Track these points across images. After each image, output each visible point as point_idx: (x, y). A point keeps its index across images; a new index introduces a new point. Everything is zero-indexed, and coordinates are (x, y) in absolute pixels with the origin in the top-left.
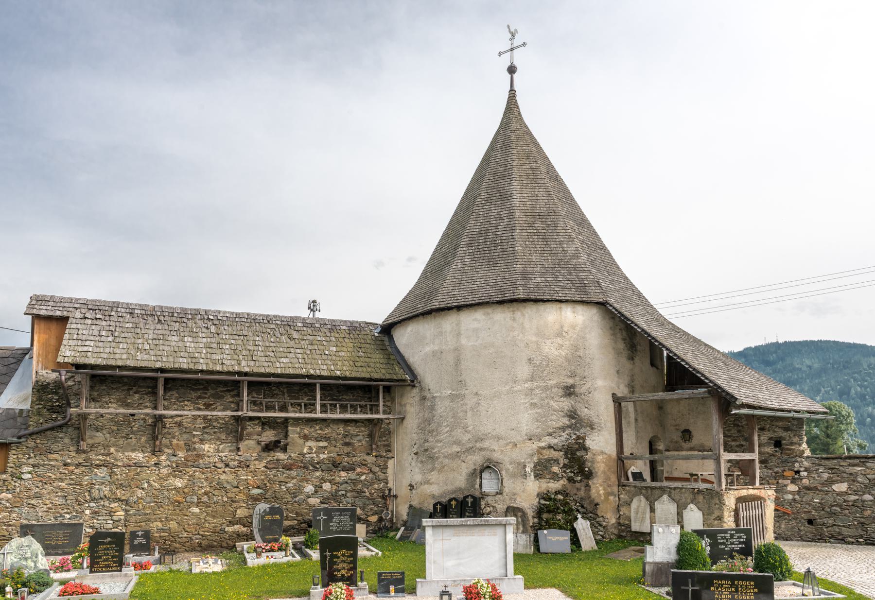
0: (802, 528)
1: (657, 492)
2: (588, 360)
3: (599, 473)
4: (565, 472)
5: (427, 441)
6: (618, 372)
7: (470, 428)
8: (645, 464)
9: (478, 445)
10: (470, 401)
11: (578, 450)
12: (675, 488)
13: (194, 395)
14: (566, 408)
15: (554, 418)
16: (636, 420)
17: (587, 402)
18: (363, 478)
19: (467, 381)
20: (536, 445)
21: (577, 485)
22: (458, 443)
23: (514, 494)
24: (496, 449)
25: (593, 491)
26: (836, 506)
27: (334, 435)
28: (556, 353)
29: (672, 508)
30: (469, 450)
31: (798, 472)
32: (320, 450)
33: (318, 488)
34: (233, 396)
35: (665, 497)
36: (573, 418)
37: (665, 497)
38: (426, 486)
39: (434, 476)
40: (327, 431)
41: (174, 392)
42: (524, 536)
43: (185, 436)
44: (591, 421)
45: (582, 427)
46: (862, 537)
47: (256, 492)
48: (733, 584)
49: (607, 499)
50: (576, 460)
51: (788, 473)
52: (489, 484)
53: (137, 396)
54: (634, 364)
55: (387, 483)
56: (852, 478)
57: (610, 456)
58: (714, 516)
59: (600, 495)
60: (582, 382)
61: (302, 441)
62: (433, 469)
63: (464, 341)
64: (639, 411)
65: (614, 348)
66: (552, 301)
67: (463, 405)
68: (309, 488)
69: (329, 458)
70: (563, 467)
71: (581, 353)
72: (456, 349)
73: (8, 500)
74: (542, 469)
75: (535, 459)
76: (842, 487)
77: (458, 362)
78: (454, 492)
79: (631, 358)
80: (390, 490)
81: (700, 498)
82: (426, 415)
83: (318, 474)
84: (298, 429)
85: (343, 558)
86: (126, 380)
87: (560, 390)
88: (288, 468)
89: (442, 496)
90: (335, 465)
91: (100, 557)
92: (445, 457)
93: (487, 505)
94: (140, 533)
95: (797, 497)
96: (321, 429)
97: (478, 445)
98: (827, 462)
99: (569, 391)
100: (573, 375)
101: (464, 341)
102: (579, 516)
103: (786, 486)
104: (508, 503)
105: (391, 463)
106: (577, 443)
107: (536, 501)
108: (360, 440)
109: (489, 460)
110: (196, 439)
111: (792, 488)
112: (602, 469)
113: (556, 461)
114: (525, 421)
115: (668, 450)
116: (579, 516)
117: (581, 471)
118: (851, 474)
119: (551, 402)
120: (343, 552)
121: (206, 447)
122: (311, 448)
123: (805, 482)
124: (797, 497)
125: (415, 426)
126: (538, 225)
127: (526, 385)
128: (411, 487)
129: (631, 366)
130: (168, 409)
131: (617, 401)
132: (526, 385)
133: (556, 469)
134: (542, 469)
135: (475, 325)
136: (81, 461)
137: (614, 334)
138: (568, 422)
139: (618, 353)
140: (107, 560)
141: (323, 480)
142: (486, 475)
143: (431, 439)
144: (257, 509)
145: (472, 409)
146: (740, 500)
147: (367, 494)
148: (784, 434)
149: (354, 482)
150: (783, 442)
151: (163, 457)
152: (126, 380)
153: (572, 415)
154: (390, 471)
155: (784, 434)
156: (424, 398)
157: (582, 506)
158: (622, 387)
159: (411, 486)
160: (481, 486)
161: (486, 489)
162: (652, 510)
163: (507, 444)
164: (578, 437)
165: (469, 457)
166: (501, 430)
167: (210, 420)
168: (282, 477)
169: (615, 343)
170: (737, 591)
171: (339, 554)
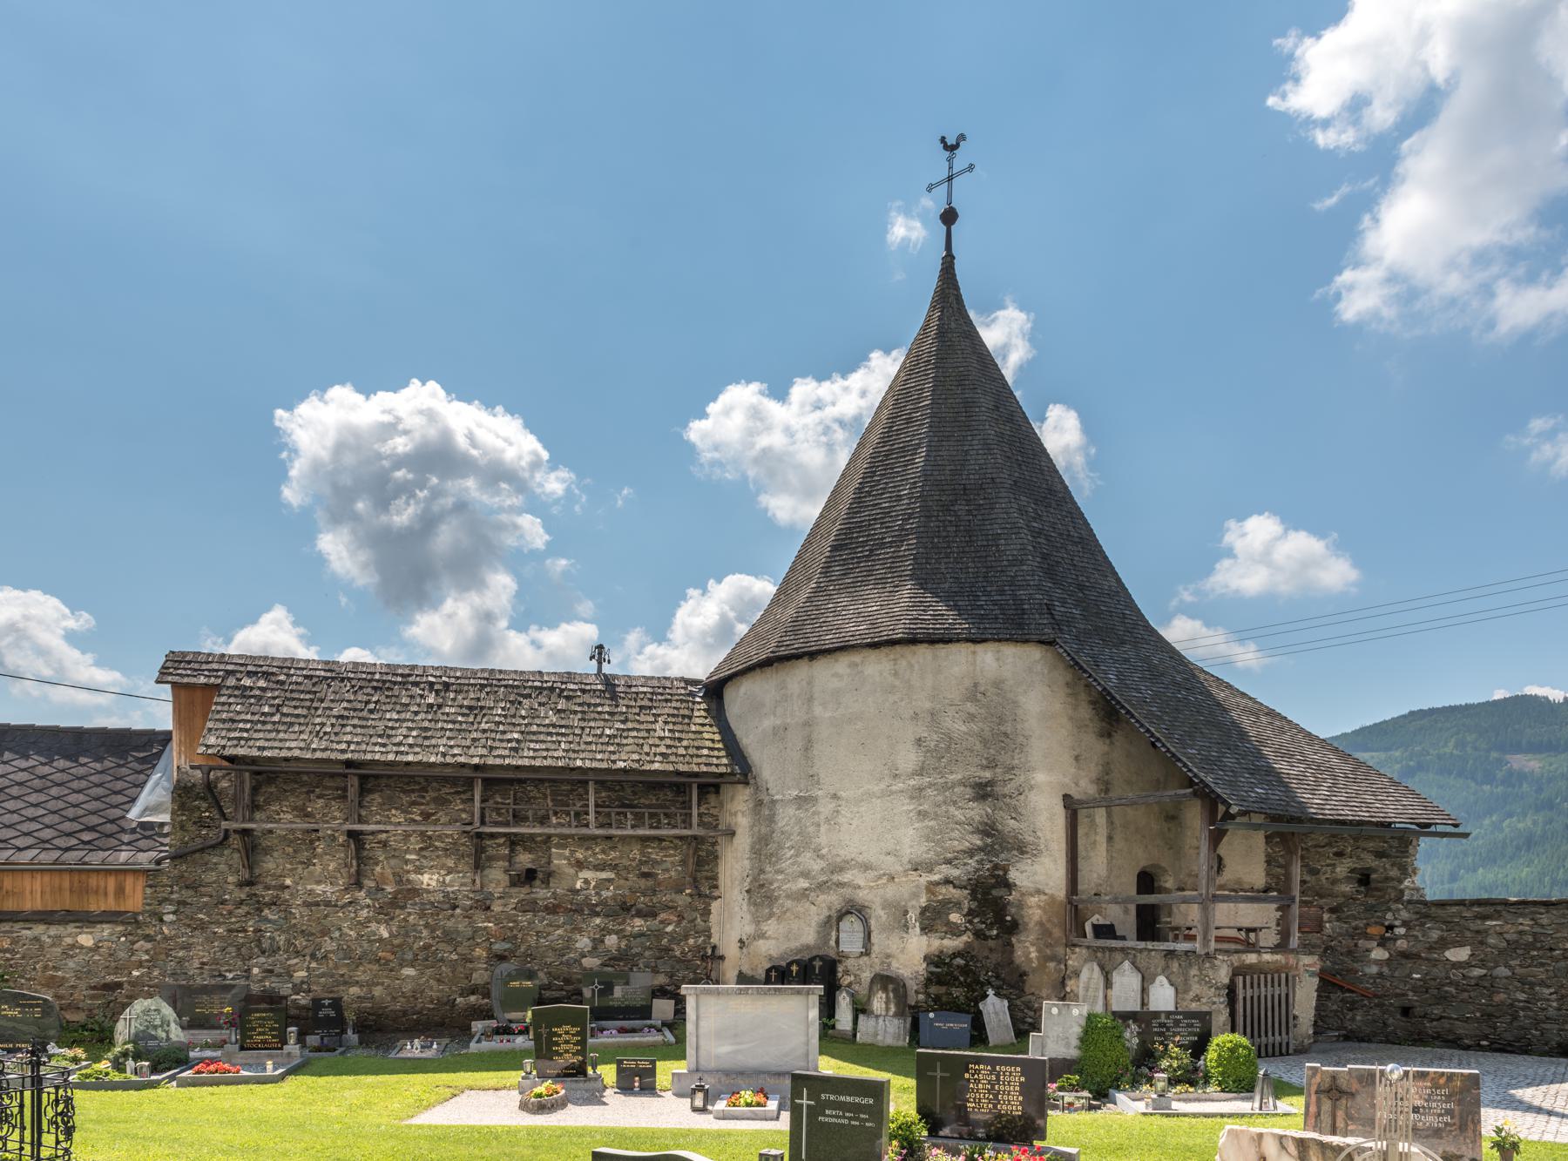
0: (1391, 1021)
2: (1020, 739)
3: (1031, 925)
4: (970, 922)
5: (762, 871)
6: (1077, 758)
7: (824, 851)
8: (1126, 911)
9: (835, 878)
10: (825, 808)
11: (994, 887)
12: (1141, 951)
13: (405, 799)
14: (977, 818)
15: (956, 834)
16: (1110, 838)
17: (1015, 809)
18: (669, 929)
19: (822, 776)
20: (926, 878)
21: (991, 943)
22: (805, 874)
23: (888, 956)
24: (862, 883)
25: (1019, 953)
26: (1451, 984)
27: (626, 862)
28: (963, 728)
30: (822, 887)
31: (1390, 928)
32: (602, 884)
33: (598, 942)
34: (463, 802)
36: (988, 835)
37: (1127, 964)
38: (761, 942)
39: (771, 927)
40: (613, 854)
41: (376, 796)
42: (896, 1021)
43: (393, 862)
44: (1021, 841)
45: (1003, 849)
46: (1486, 1037)
47: (499, 947)
48: (994, 1069)
49: (1042, 966)
50: (990, 900)
51: (1374, 930)
52: (850, 939)
53: (321, 802)
54: (1112, 743)
55: (709, 937)
56: (1479, 939)
57: (1052, 897)
58: (1192, 994)
59: (1030, 961)
60: (1008, 777)
61: (572, 871)
62: (771, 915)
63: (818, 710)
64: (1117, 822)
65: (1071, 718)
66: (797, 657)
67: (814, 813)
68: (583, 943)
69: (614, 898)
70: (968, 914)
71: (1008, 728)
72: (807, 724)
73: (147, 952)
74: (932, 919)
75: (923, 901)
76: (1460, 954)
78: (799, 951)
79: (1106, 734)
81: (1175, 966)
82: (764, 830)
83: (598, 921)
84: (567, 852)
85: (567, 1037)
86: (305, 778)
87: (968, 790)
88: (552, 910)
89: (782, 958)
90: (625, 909)
91: (254, 1029)
92: (788, 897)
93: (847, 972)
94: (327, 1002)
95: (1385, 970)
96: (603, 852)
97: (835, 878)
98: (1440, 912)
99: (983, 791)
100: (991, 764)
102: (991, 992)
103: (1369, 951)
104: (878, 969)
105: (715, 906)
106: (993, 876)
107: (922, 967)
108: (667, 870)
110: (409, 867)
111: (1379, 954)
112: (1036, 918)
113: (957, 905)
114: (910, 841)
115: (1181, 889)
116: (991, 992)
117: (999, 919)
118: (1478, 932)
119: (952, 809)
120: (567, 1028)
121: (426, 878)
122: (586, 881)
123: (1402, 944)
124: (1385, 970)
125: (747, 848)
126: (961, 508)
127: (912, 782)
129: (1106, 748)
130: (367, 822)
131: (1072, 807)
132: (912, 782)
133: (955, 917)
134: (932, 919)
135: (835, 684)
136: (243, 896)
137: (1074, 695)
138: (979, 843)
139: (1080, 726)
140: (263, 1034)
141: (605, 931)
143: (768, 869)
144: (497, 971)
145: (827, 820)
146: (1236, 972)
147: (678, 953)
149: (659, 934)
150: (1374, 876)
151: (362, 894)
152: (305, 778)
153: (988, 830)
154: (713, 918)
156: (760, 803)
157: (997, 977)
158: (1084, 783)
159: (741, 941)
161: (843, 947)
162: (1108, 984)
163: (880, 877)
164: (996, 867)
165: (822, 897)
166: (871, 854)
167: (430, 838)
168: (539, 926)
169: (1075, 708)
170: (998, 1079)
171: (559, 1031)
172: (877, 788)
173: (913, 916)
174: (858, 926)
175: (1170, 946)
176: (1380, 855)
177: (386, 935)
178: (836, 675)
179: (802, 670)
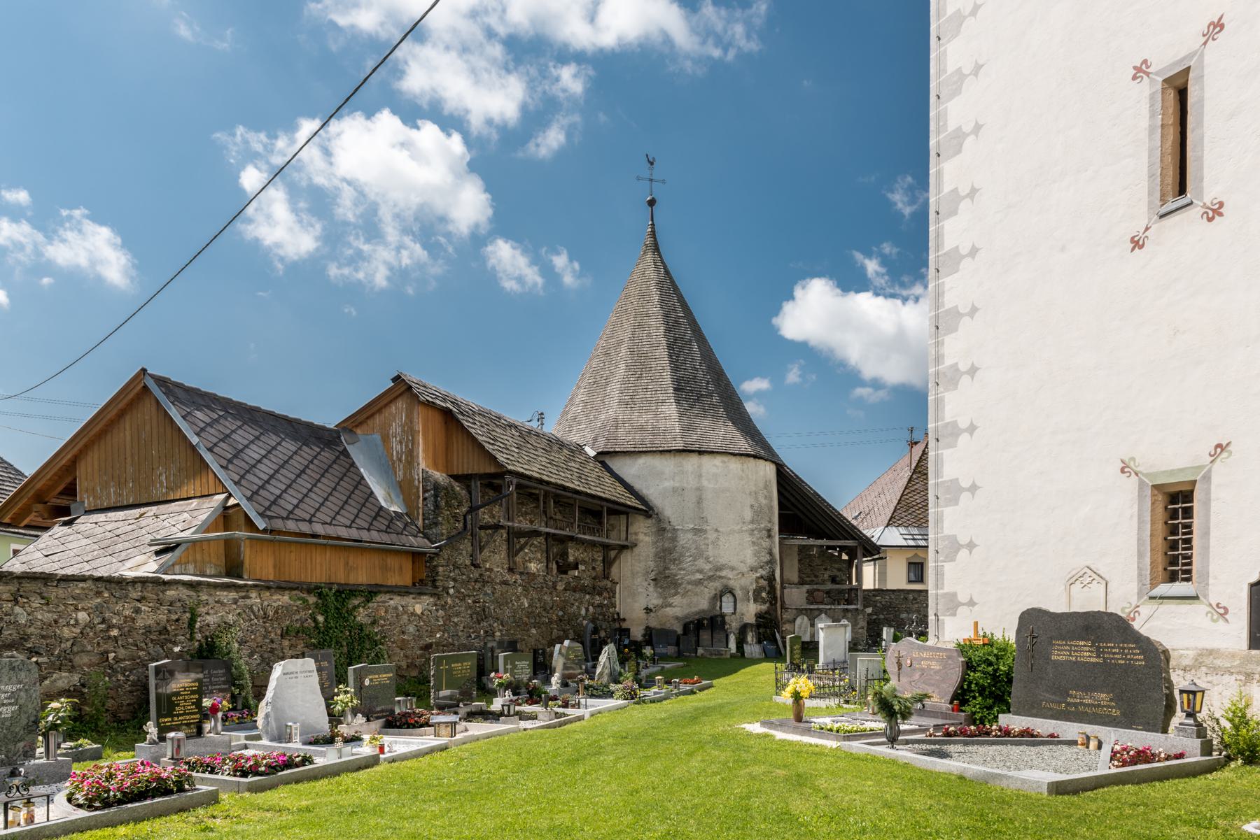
10: (712, 536)
22: (700, 571)
30: (711, 578)
39: (676, 600)
52: (727, 607)
62: (676, 594)
77: (700, 501)
81: (849, 615)
92: (689, 583)
101: (705, 483)
128: (648, 610)
135: (714, 470)
142: (724, 599)
159: (647, 609)
162: (813, 625)
166: (734, 562)
172: (737, 528)
173: (751, 593)
174: (731, 599)
176: (839, 570)
177: (419, 611)
179: (694, 460)
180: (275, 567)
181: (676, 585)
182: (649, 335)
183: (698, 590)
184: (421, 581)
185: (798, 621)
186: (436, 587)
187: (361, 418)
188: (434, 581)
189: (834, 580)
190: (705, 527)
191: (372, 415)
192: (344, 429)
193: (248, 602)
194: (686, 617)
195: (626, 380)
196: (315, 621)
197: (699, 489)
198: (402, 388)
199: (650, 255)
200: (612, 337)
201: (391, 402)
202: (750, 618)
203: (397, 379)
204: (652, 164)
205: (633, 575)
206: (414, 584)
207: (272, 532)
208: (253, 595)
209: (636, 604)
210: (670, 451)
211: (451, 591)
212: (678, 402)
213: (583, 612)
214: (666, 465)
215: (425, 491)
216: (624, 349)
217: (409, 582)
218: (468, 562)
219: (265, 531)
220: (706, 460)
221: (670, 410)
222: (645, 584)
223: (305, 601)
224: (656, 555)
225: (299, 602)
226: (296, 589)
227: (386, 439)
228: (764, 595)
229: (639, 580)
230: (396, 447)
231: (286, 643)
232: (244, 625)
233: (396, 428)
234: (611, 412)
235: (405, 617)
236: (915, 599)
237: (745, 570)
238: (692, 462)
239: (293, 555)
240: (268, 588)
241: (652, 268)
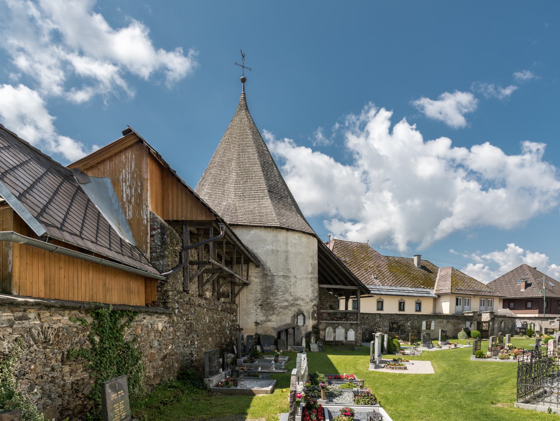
1: (336, 325)
9: (296, 302)
10: (293, 280)
19: (292, 270)
22: (287, 301)
29: (343, 331)
30: (292, 305)
35: (340, 327)
38: (269, 323)
39: (274, 318)
52: (300, 323)
62: (274, 314)
77: (287, 259)
80: (239, 326)
81: (354, 326)
82: (268, 284)
92: (281, 308)
97: (296, 302)
101: (290, 248)
109: (300, 310)
128: (257, 324)
135: (294, 241)
142: (299, 317)
143: (271, 298)
145: (293, 284)
148: (333, 304)
155: (333, 304)
159: (256, 323)
160: (297, 322)
162: (335, 332)
166: (303, 296)
172: (305, 276)
175: (351, 322)
178: (295, 238)
179: (284, 233)
180: (45, 283)
181: (273, 308)
182: (249, 157)
183: (285, 312)
184: (153, 302)
185: (327, 330)
186: (167, 308)
187: (92, 163)
188: (165, 303)
189: (331, 307)
190: (289, 275)
191: (103, 161)
192: (76, 170)
193: (26, 324)
194: (279, 328)
195: (237, 183)
196: (92, 342)
197: (286, 252)
198: (132, 140)
199: (243, 111)
200: (224, 156)
201: (121, 152)
202: (310, 329)
203: (128, 132)
204: (243, 57)
205: (248, 302)
206: (147, 305)
207: (51, 240)
208: (32, 315)
209: (250, 320)
210: (270, 227)
211: (176, 311)
212: (271, 198)
213: (227, 325)
214: (269, 235)
215: (152, 229)
216: (234, 164)
217: (143, 304)
218: (181, 289)
219: (43, 238)
220: (290, 234)
221: (267, 202)
222: (255, 307)
223: (83, 321)
224: (262, 290)
225: (79, 323)
226: (74, 308)
227: (116, 183)
228: (315, 315)
229: (251, 305)
230: (126, 191)
231: (67, 369)
232: (23, 353)
233: (125, 174)
234: (230, 200)
235: (153, 334)
236: (367, 318)
237: (308, 301)
238: (283, 235)
239: (62, 271)
240: (48, 307)
241: (246, 119)
